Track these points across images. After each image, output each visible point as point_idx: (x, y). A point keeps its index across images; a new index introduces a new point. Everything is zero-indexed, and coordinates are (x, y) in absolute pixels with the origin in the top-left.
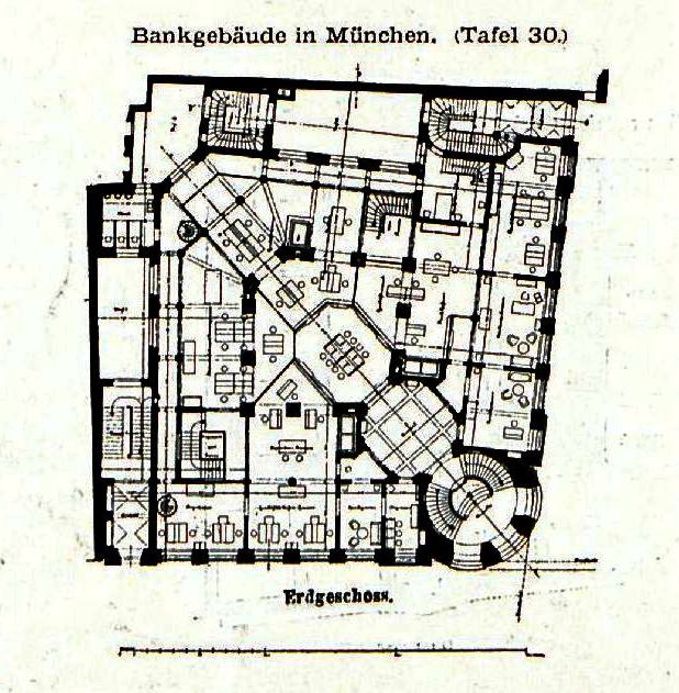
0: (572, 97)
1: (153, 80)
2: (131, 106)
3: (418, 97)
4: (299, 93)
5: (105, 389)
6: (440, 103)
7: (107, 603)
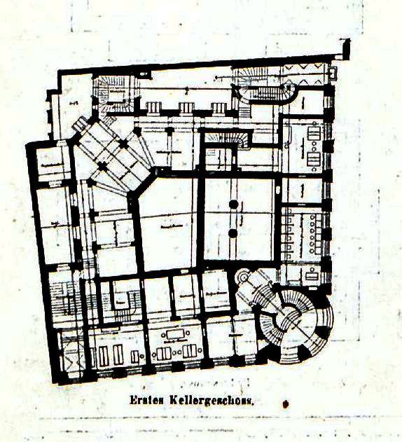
1: (61, 73)
4: (153, 73)
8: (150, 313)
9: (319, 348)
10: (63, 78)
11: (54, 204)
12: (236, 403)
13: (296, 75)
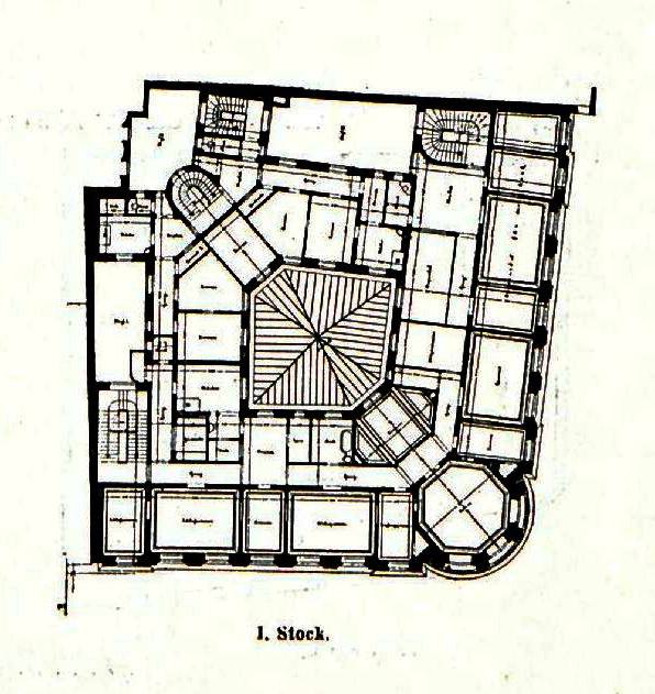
0: (564, 112)
1: (149, 85)
2: (129, 113)
3: (414, 107)
4: (293, 100)
5: (101, 392)
6: (432, 115)
7: (91, 671)
8: (318, 471)
9: (462, 574)
10: (153, 92)
11: (121, 286)
12: (303, 633)
13: (520, 128)
